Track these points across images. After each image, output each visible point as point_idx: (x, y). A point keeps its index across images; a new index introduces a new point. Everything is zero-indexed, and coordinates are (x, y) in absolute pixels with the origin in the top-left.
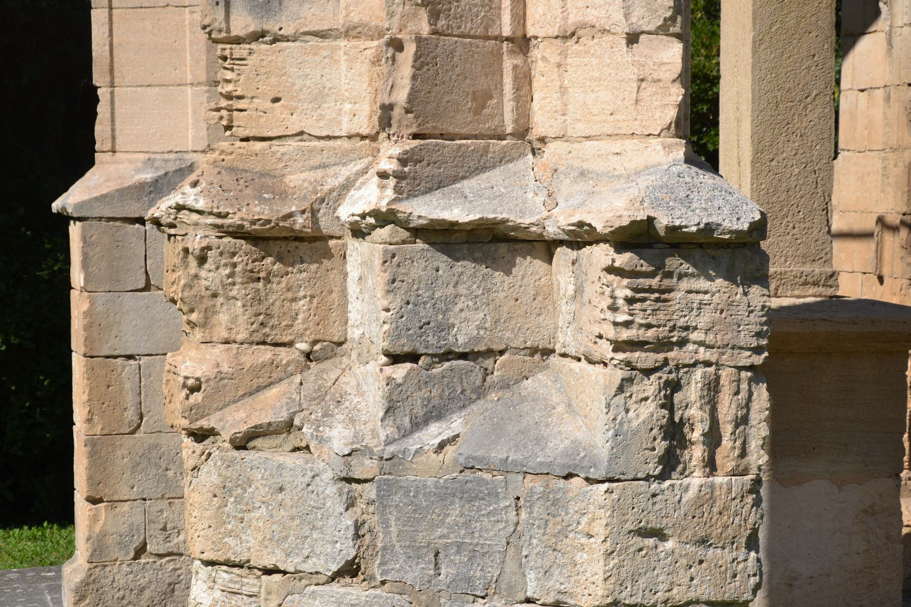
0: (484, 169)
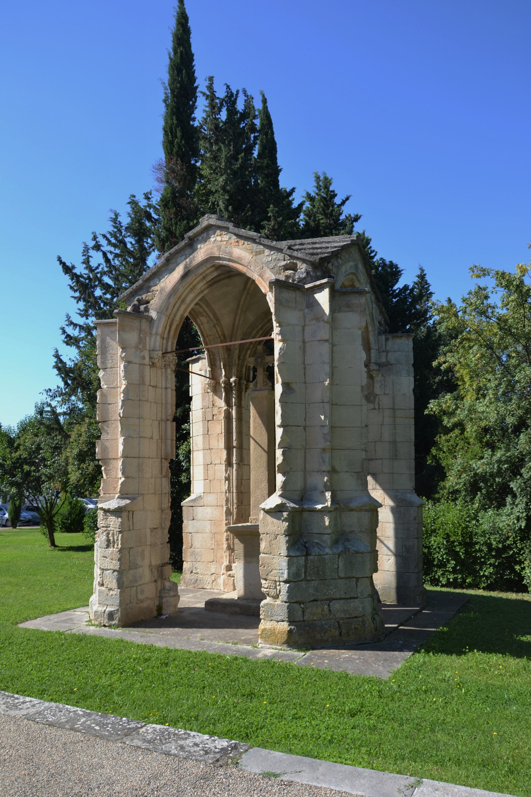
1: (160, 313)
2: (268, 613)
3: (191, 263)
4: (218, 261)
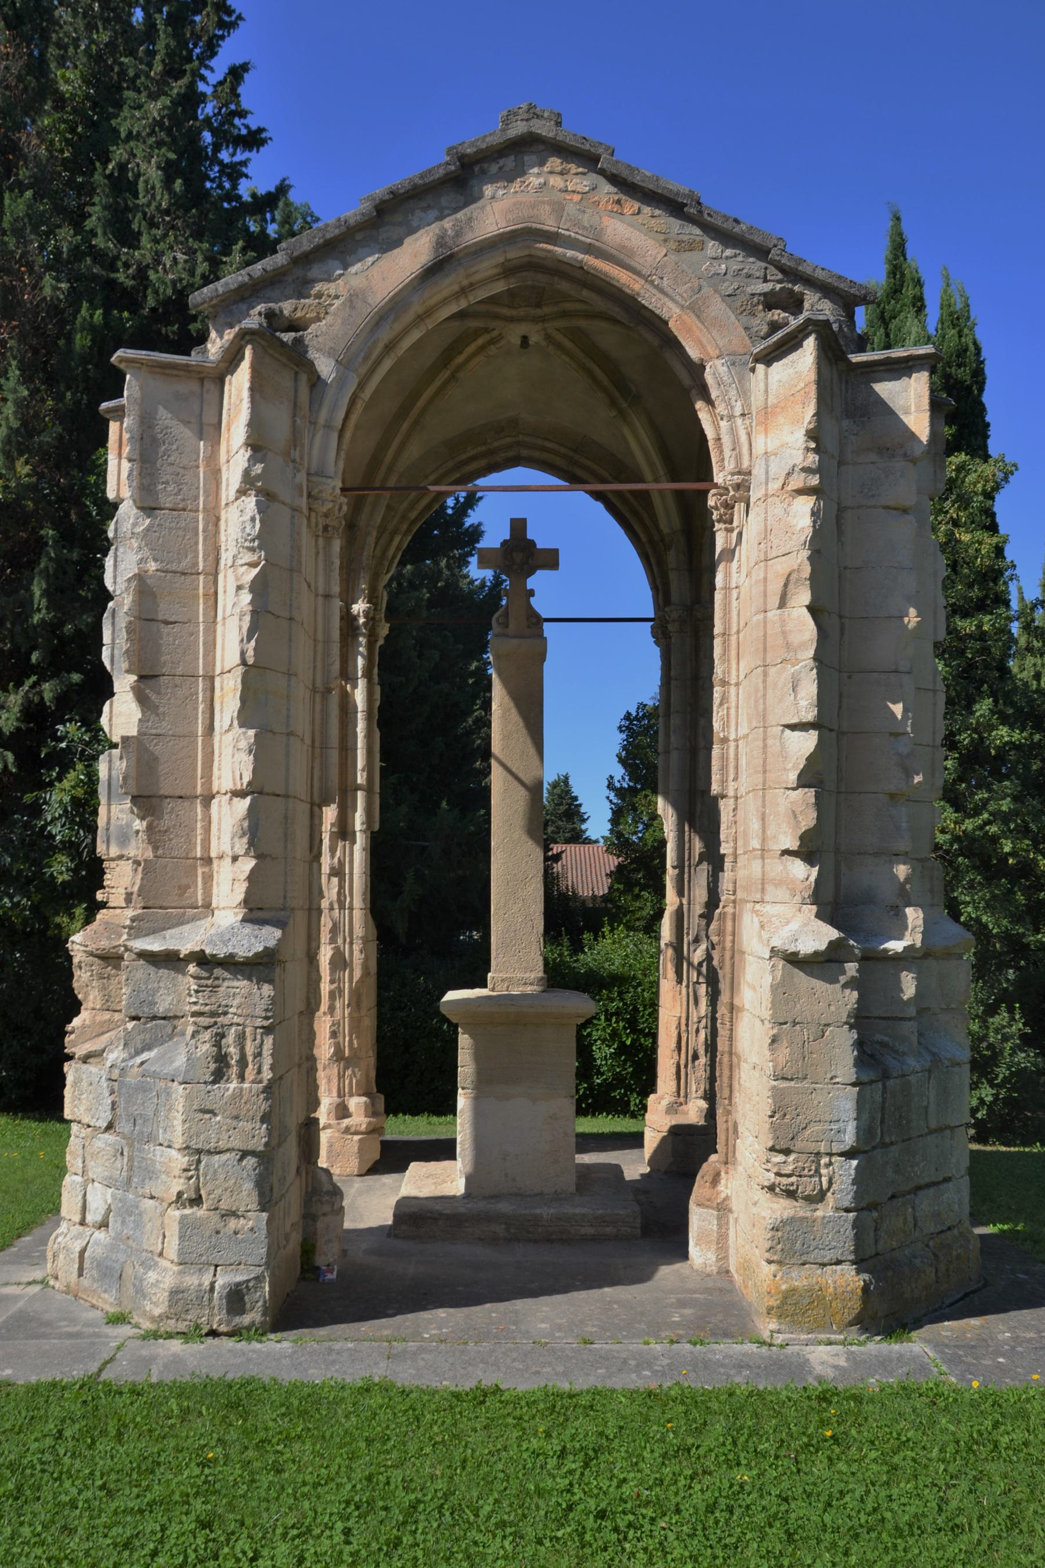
0: (182, 924)
1: (343, 364)
2: (793, 1244)
3: (458, 234)
4: (545, 246)
